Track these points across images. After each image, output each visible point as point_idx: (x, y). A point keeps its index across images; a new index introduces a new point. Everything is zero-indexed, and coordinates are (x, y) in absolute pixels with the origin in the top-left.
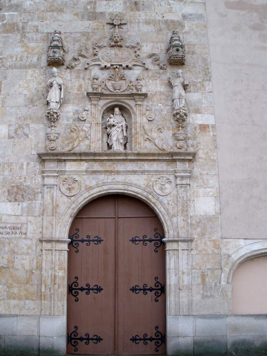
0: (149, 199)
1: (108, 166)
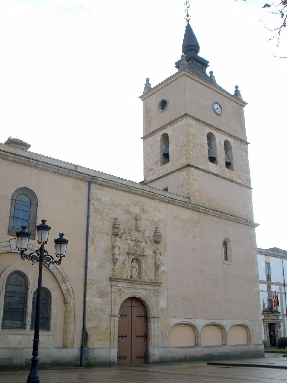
0: (146, 300)
1: (134, 286)
